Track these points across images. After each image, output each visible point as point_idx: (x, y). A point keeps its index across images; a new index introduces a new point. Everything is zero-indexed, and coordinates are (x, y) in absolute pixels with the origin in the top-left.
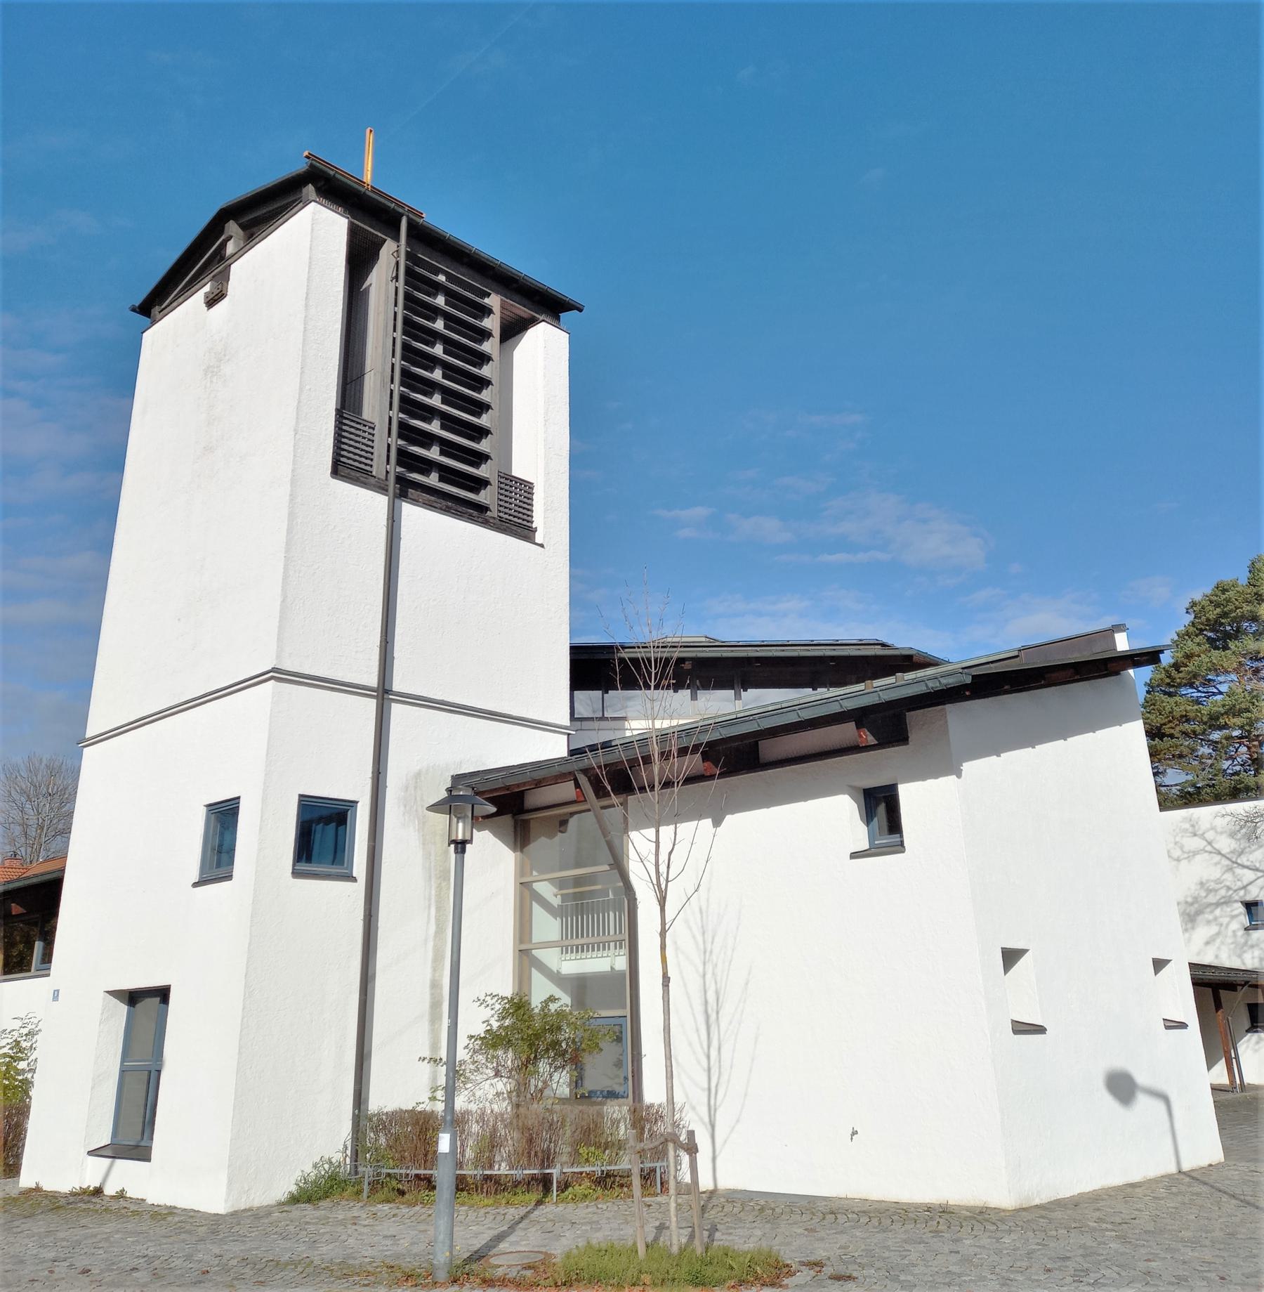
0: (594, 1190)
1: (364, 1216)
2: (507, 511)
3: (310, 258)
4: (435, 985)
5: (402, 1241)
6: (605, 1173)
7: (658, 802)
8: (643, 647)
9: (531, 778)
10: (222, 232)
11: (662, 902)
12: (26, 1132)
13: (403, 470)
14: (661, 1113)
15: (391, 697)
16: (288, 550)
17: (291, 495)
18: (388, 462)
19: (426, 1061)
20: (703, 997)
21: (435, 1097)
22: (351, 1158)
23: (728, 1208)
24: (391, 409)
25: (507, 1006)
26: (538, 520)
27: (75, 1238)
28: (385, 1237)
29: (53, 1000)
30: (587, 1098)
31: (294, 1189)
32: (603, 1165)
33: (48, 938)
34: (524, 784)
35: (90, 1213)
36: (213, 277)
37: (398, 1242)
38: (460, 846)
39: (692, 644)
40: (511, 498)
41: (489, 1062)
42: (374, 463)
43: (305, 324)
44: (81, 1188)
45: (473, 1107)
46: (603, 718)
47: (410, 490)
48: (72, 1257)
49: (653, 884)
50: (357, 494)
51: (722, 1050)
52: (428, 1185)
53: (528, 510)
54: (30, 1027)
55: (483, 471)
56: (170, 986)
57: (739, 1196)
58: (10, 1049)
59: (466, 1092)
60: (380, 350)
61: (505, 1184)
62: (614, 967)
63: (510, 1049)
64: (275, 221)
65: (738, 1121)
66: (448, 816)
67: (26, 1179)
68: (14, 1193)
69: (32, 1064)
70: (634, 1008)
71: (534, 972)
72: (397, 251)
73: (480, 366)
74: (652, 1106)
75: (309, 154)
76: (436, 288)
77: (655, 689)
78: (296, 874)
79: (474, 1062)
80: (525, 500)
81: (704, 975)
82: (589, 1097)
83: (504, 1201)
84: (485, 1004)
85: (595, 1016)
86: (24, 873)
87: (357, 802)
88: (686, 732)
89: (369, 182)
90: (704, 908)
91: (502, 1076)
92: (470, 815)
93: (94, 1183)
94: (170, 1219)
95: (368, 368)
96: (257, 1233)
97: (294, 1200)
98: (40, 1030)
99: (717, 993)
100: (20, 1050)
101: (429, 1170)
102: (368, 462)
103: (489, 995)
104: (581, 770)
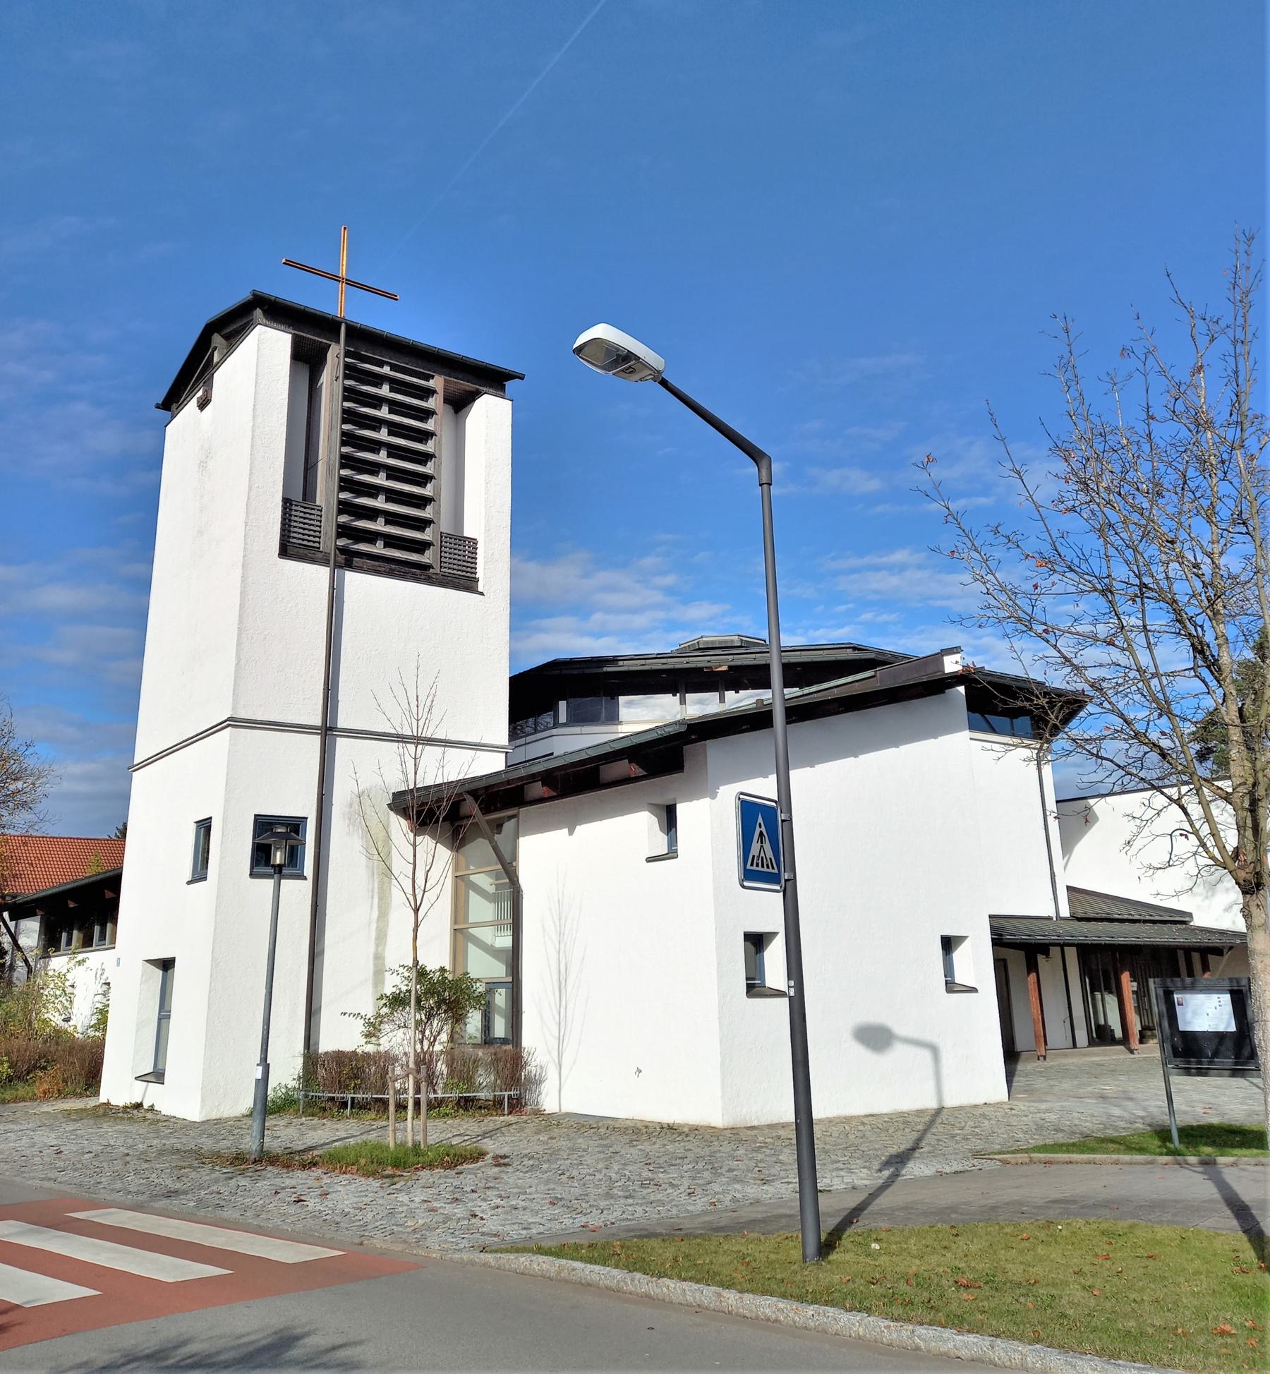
16: (240, 622)
17: (243, 577)
19: (347, 1015)
67: (103, 1098)
78: (253, 875)
87: (306, 818)
89: (344, 277)
95: (320, 458)
99: (566, 965)
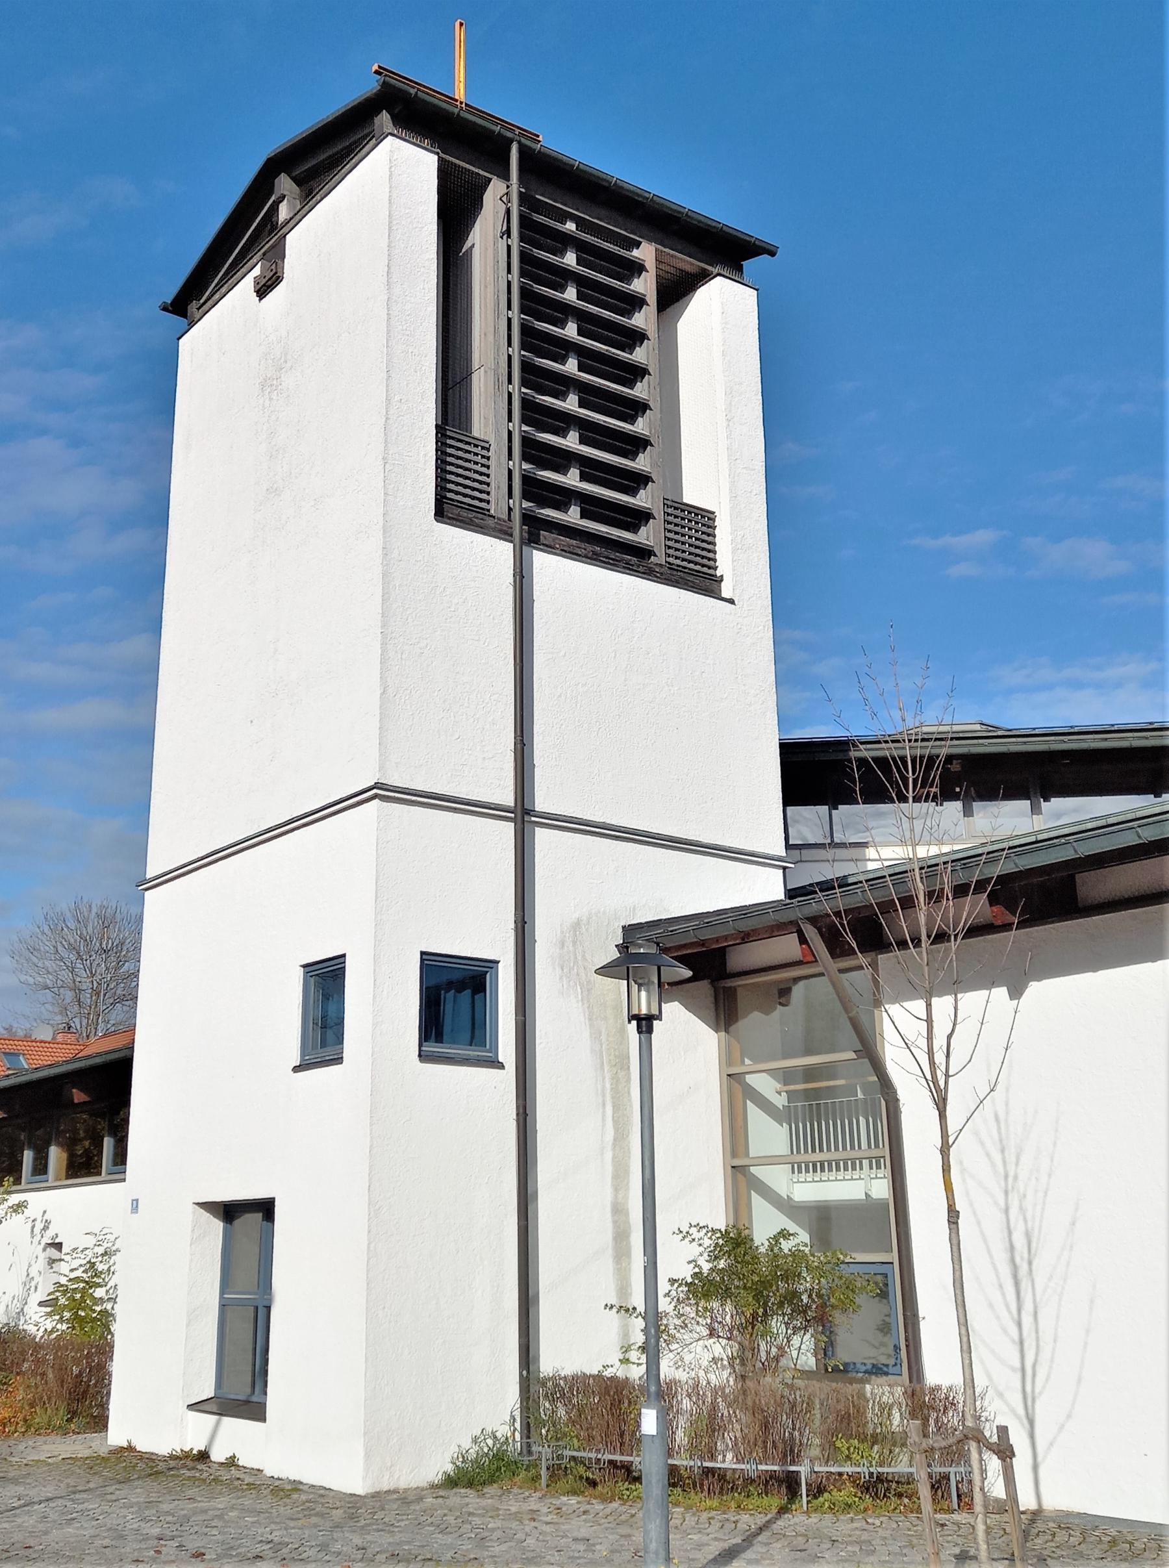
0: (860, 1498)
1: (545, 1510)
2: (678, 554)
3: (390, 216)
4: (619, 1210)
5: (598, 1547)
6: (875, 1476)
7: (928, 964)
8: (893, 741)
9: (735, 930)
10: (271, 192)
11: (941, 1104)
12: (110, 1376)
13: (532, 504)
14: (953, 1400)
15: (533, 819)
18: (510, 496)
19: (615, 1310)
20: (1007, 1239)
21: (628, 1360)
22: (521, 1433)
23: (1061, 1537)
24: (510, 420)
25: (721, 1242)
26: (724, 564)
27: (183, 1512)
28: (575, 1539)
29: (132, 1213)
30: (843, 1372)
31: (449, 1468)
32: (871, 1466)
33: (120, 1132)
34: (726, 938)
35: (197, 1482)
36: (264, 254)
37: (594, 1548)
38: (644, 1022)
39: (961, 735)
40: (683, 535)
41: (700, 1317)
42: (492, 498)
43: (388, 309)
44: (182, 1451)
45: (681, 1375)
46: (833, 845)
47: (542, 532)
48: (181, 1536)
49: (926, 1080)
50: (472, 542)
51: (1040, 1315)
52: (628, 1475)
53: (709, 551)
54: (105, 1245)
55: (642, 500)
56: (274, 1198)
57: (1077, 1521)
58: (83, 1272)
59: (671, 1355)
60: (491, 338)
61: (733, 1482)
62: (870, 1193)
63: (729, 1301)
64: (340, 168)
65: (1069, 1416)
66: (626, 982)
67: (117, 1434)
68: (103, 1452)
69: (111, 1291)
70: (904, 1253)
71: (755, 1197)
72: (507, 194)
73: (630, 348)
74: (938, 1388)
75: (379, 67)
76: (564, 242)
77: (914, 802)
78: (423, 1057)
79: (679, 1316)
80: (705, 537)
81: (1007, 1210)
82: (846, 1371)
83: (733, 1505)
84: (690, 1238)
85: (846, 1261)
86: (82, 1050)
87: (498, 962)
88: (964, 861)
89: (463, 100)
90: (1002, 1116)
91: (719, 1336)
92: (656, 981)
93: (198, 1446)
94: (295, 1496)
95: (476, 364)
96: (407, 1523)
97: (451, 1482)
98: (118, 1250)
99: (1028, 1235)
100: (96, 1274)
101: (628, 1455)
102: (484, 496)
103: (695, 1226)
104: (807, 918)
